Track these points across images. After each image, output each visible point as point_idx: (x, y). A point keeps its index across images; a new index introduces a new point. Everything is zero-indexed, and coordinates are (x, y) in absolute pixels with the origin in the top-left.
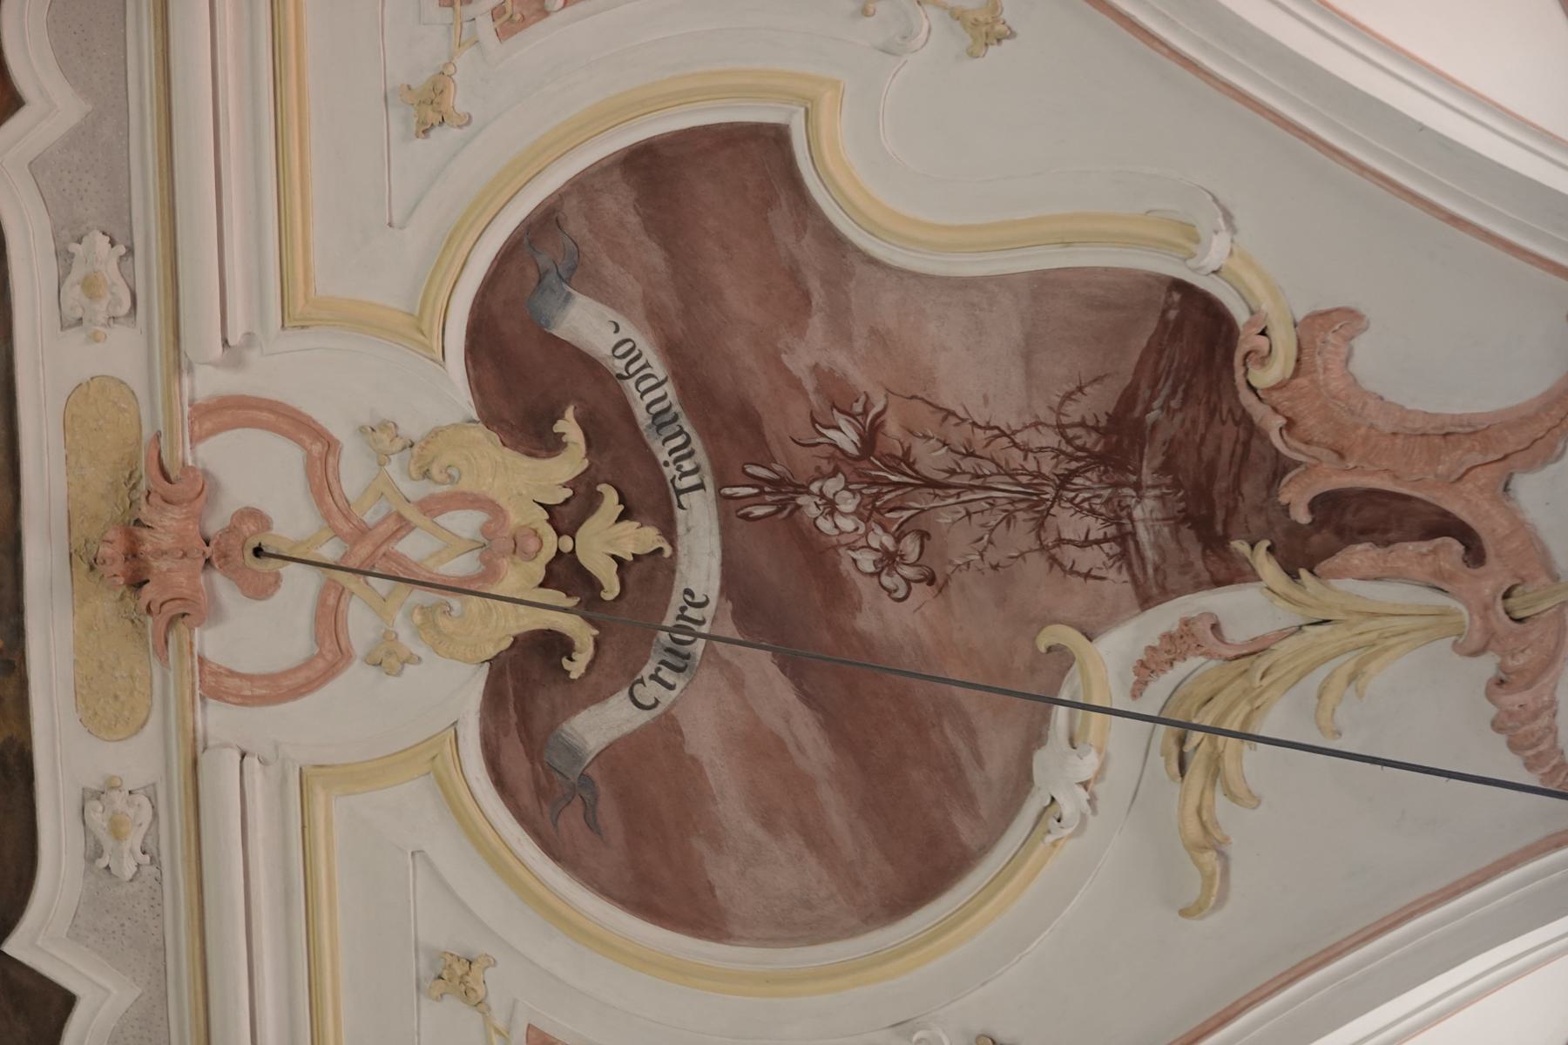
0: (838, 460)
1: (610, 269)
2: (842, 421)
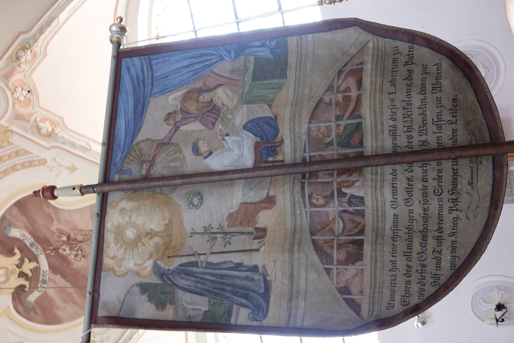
0: (64, 242)
1: (17, 223)
2: (63, 236)
